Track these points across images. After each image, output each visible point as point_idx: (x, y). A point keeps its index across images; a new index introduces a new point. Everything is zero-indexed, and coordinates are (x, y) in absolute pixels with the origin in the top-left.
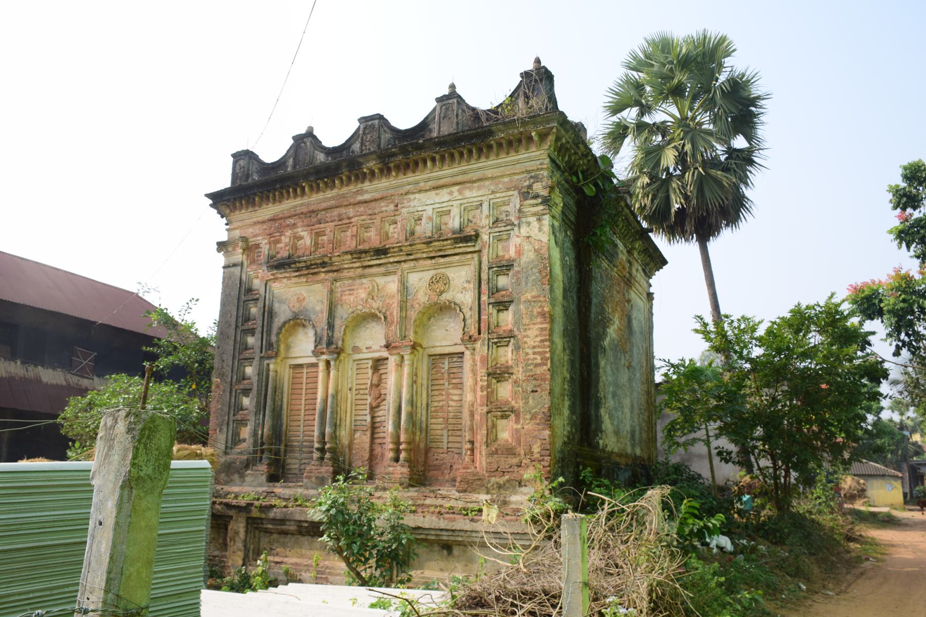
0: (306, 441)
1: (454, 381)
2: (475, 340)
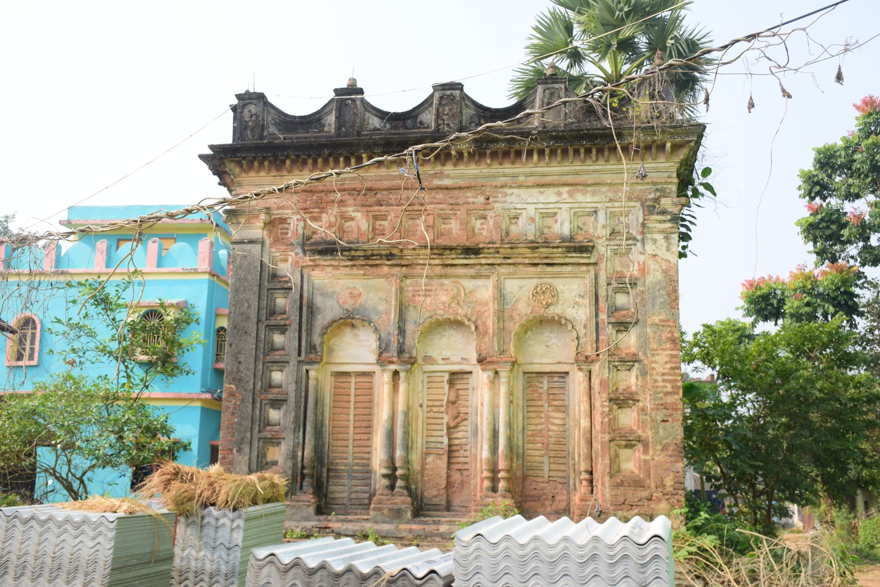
0: (357, 465)
1: (555, 403)
2: (592, 362)
